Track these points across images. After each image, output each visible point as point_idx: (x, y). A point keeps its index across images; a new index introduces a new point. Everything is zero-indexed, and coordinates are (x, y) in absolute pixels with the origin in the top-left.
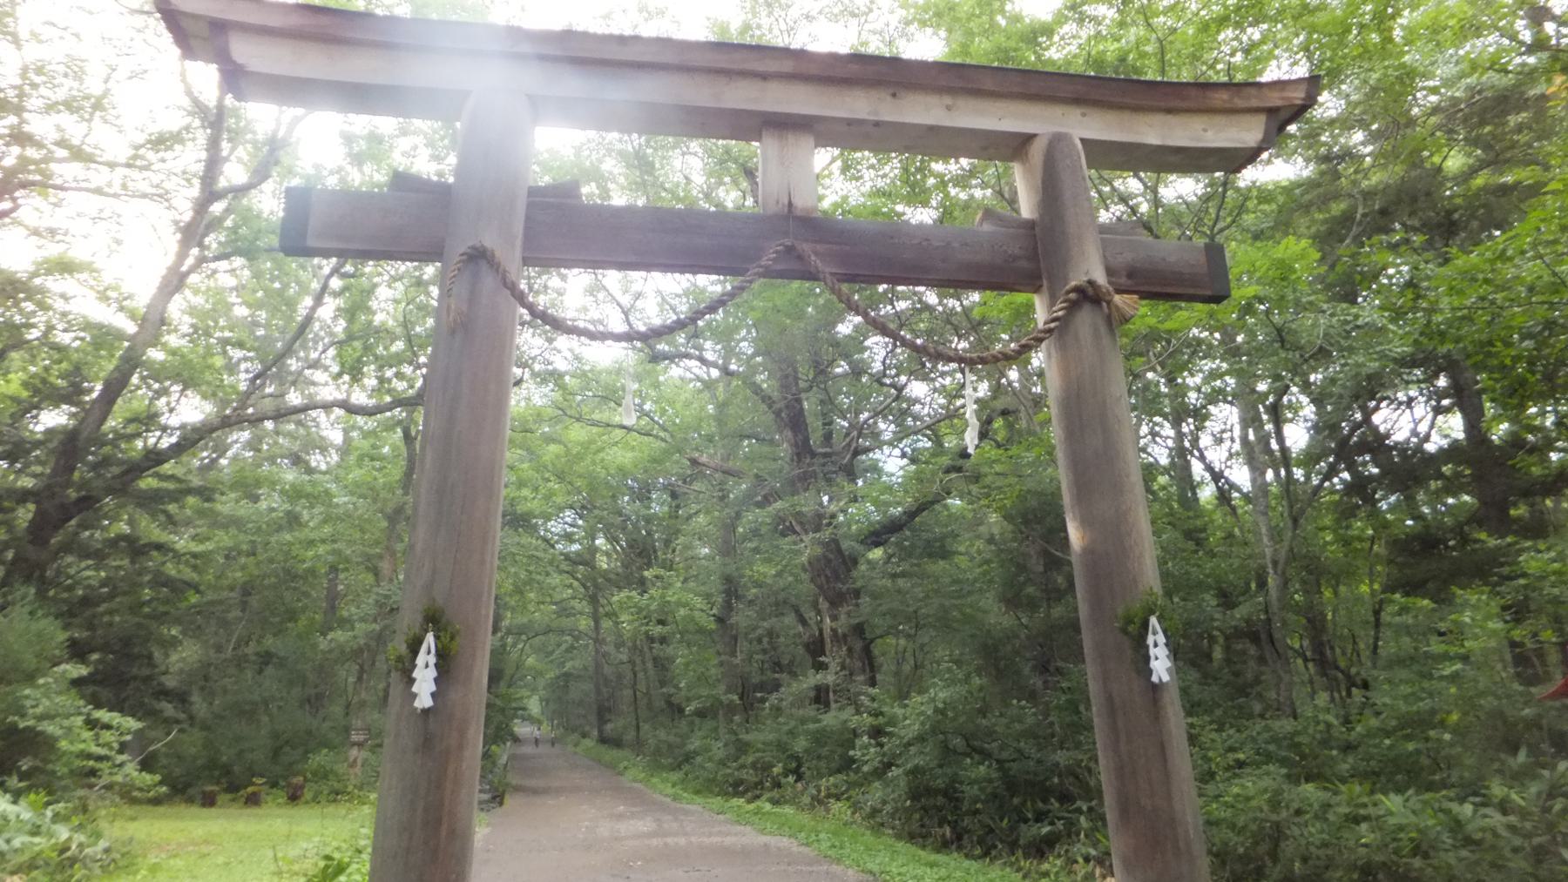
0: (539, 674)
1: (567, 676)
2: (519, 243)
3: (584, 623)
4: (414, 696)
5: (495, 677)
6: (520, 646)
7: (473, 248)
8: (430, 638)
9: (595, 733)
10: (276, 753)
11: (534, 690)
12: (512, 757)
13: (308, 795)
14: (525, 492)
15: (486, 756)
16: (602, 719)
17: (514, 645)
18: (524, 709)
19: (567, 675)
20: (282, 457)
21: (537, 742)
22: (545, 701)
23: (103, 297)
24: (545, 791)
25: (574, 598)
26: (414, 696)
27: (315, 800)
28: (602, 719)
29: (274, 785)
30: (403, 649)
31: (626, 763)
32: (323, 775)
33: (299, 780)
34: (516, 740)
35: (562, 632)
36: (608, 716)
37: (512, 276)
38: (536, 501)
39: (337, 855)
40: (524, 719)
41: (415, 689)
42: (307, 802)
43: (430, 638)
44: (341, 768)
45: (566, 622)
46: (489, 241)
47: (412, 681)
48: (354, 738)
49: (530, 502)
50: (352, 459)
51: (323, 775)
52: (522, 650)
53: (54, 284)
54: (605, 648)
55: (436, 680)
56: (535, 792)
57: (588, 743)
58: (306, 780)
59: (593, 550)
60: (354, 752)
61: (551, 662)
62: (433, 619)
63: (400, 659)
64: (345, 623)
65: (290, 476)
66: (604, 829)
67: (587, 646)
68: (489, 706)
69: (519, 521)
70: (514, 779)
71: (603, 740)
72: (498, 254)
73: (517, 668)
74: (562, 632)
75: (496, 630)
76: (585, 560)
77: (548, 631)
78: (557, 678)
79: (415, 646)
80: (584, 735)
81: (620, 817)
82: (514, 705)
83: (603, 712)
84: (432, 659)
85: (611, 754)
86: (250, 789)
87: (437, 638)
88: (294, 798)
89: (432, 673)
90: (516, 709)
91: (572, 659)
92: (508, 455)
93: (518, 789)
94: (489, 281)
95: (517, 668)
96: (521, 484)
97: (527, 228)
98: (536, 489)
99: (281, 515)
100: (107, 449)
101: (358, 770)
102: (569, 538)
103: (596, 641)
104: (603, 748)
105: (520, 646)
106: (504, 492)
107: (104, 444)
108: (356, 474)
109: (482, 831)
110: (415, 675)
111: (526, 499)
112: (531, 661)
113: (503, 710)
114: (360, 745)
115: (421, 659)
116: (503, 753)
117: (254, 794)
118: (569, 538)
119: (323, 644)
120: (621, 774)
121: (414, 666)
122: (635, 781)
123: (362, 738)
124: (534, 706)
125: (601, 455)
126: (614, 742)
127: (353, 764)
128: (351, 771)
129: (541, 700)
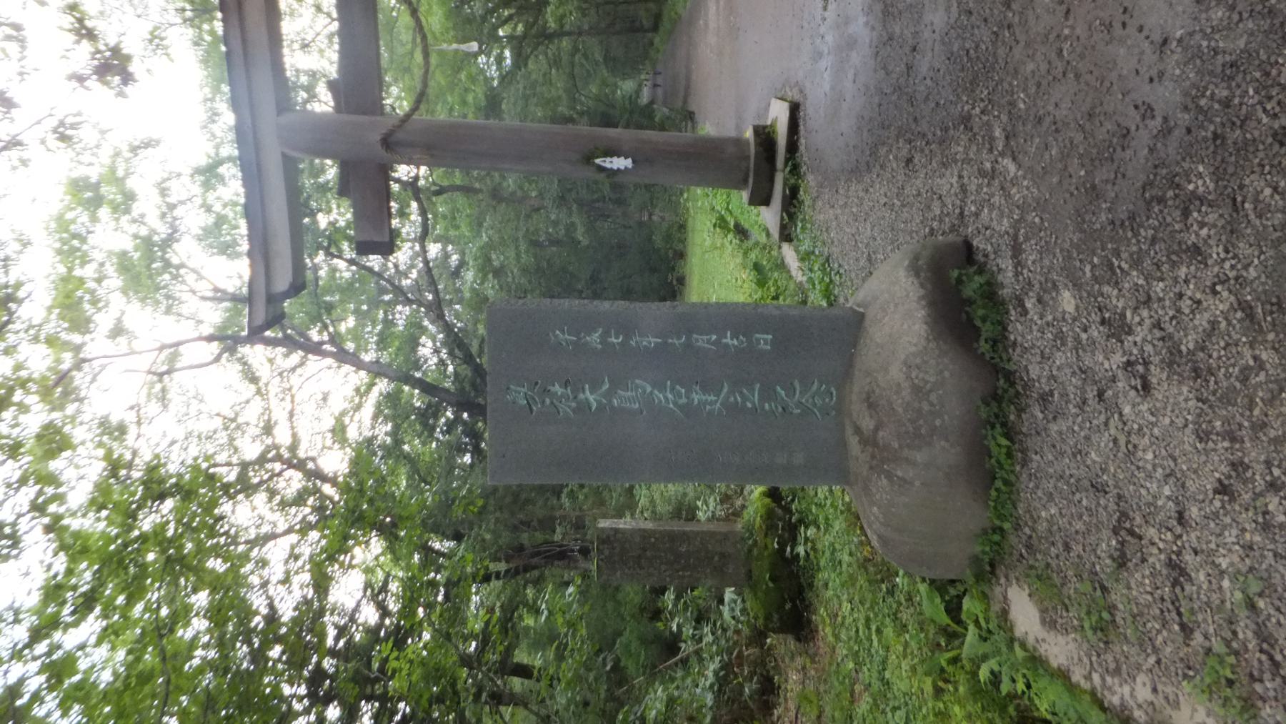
0: (604, 84)
1: (607, 59)
2: (373, 118)
3: (565, 43)
4: (626, 168)
5: (608, 122)
6: (583, 98)
7: (382, 145)
8: (598, 161)
9: (650, 35)
10: (653, 270)
11: (616, 86)
12: (665, 103)
13: (681, 246)
14: (470, 98)
15: (662, 128)
16: (640, 29)
17: (582, 104)
18: (631, 97)
19: (606, 58)
20: (455, 284)
21: (655, 86)
22: (625, 77)
23: (358, 408)
24: (688, 79)
25: (546, 55)
26: (626, 168)
27: (683, 241)
28: (640, 29)
29: (673, 269)
30: (603, 175)
31: (673, 13)
32: (668, 238)
33: (671, 254)
34: (652, 102)
35: (572, 65)
36: (637, 24)
37: (396, 122)
38: (477, 90)
39: (714, 221)
40: (638, 97)
41: (622, 168)
42: (685, 247)
43: (598, 161)
44: (665, 225)
45: (565, 58)
46: (376, 137)
47: (619, 169)
48: (646, 218)
49: (477, 94)
50: (452, 233)
51: (668, 238)
52: (586, 97)
53: (352, 434)
54: (586, 27)
55: (619, 157)
56: (688, 88)
57: (657, 40)
58: (671, 248)
59: (511, 38)
60: (655, 218)
61: (594, 71)
62: (588, 159)
63: (608, 177)
64: (571, 228)
65: (469, 275)
66: (712, 39)
67: (583, 41)
68: (627, 126)
69: (492, 104)
70: (679, 104)
71: (655, 28)
72: (384, 131)
73: (600, 100)
74: (572, 65)
75: (570, 120)
76: (517, 44)
77: (572, 76)
78: (607, 67)
79: (601, 169)
80: (652, 44)
81: (706, 25)
82: (627, 102)
83: (634, 28)
84: (608, 159)
85: (666, 24)
86: (675, 282)
87: (597, 157)
88: (681, 255)
89: (615, 159)
90: (630, 103)
91: (593, 54)
92: (442, 117)
93: (685, 102)
94: (400, 136)
95: (600, 100)
96: (464, 103)
97: (364, 113)
98: (466, 90)
99: (496, 281)
100: (468, 388)
101: (666, 215)
102: (500, 59)
103: (580, 34)
104: (661, 29)
105: (583, 98)
106: (471, 118)
107: (463, 388)
108: (465, 230)
109: (708, 128)
110: (615, 168)
111: (474, 98)
112: (594, 89)
113: (631, 112)
114: (650, 215)
115: (608, 165)
116: (661, 111)
117: (677, 280)
118: (500, 59)
119: (585, 242)
120: (680, 17)
121: (612, 169)
122: (685, 7)
123: (646, 213)
124: (628, 86)
125: (438, 35)
126: (658, 18)
127: (663, 218)
128: (667, 219)
129: (624, 79)
